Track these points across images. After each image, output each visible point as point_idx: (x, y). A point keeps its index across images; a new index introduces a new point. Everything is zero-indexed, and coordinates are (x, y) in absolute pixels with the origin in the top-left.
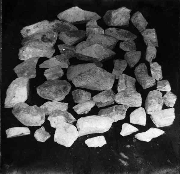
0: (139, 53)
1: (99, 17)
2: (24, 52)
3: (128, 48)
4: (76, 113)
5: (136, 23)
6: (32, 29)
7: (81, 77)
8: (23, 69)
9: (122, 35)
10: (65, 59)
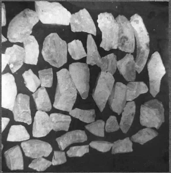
0: (102, 135)
1: (154, 94)
2: (106, 18)
3: (109, 125)
5: (142, 133)
6: (138, 26)
7: (68, 78)
8: (83, 19)
9: (127, 118)
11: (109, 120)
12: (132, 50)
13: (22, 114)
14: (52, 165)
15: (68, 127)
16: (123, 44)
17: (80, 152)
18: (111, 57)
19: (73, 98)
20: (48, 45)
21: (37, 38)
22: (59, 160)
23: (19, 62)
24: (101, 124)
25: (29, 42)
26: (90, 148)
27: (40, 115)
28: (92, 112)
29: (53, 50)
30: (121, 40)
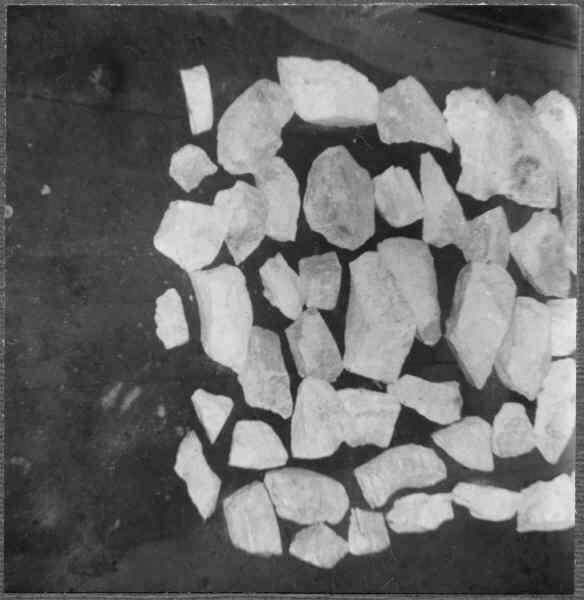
0: (488, 466)
2: (473, 103)
4: (262, 264)
7: (384, 279)
8: (411, 105)
10: (451, 231)
11: (499, 418)
12: (550, 202)
13: (261, 386)
14: (349, 555)
15: (389, 431)
16: (524, 182)
17: (427, 514)
18: (495, 217)
19: (404, 337)
20: (323, 180)
21: (291, 164)
22: (367, 539)
23: (255, 232)
24: (477, 426)
25: (271, 175)
26: (460, 511)
27: (315, 390)
28: (450, 390)
29: (340, 196)
30: (516, 170)
